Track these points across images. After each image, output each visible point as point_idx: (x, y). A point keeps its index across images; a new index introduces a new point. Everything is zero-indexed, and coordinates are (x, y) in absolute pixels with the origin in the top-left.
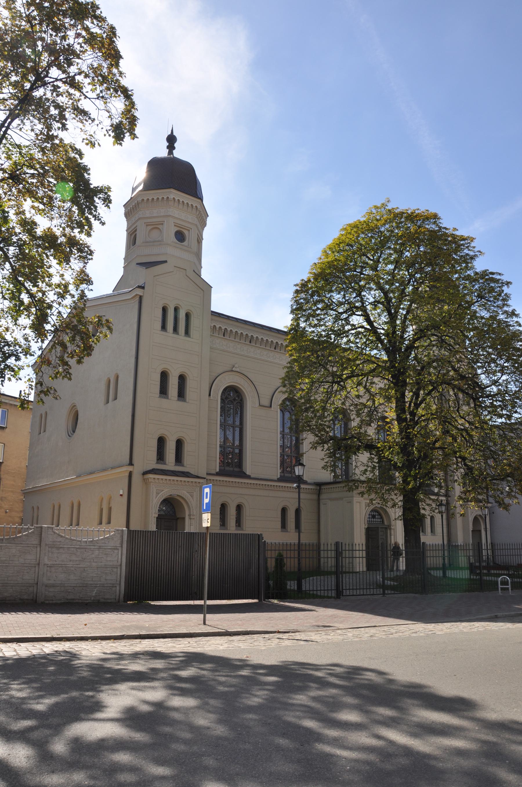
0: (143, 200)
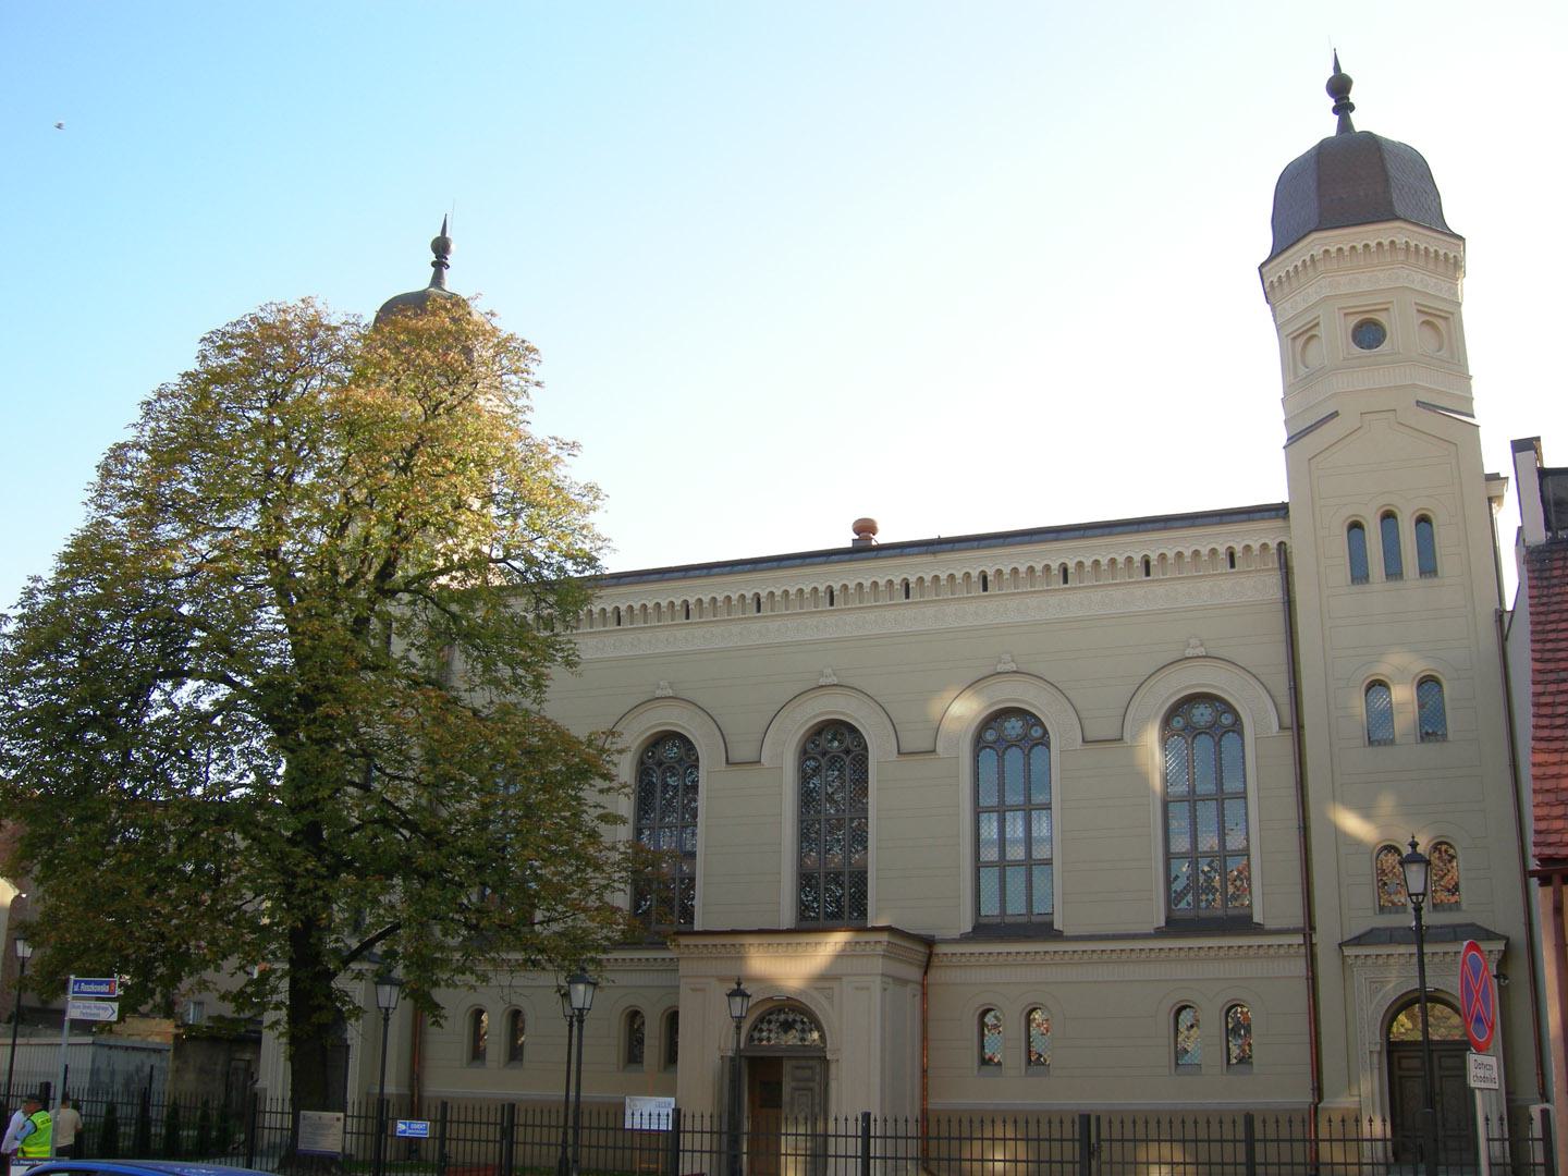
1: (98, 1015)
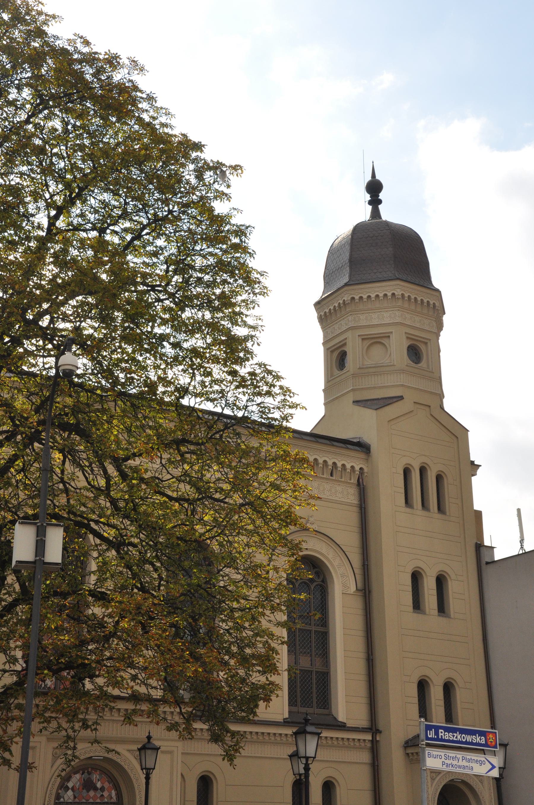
0: (353, 298)
1: (472, 768)
